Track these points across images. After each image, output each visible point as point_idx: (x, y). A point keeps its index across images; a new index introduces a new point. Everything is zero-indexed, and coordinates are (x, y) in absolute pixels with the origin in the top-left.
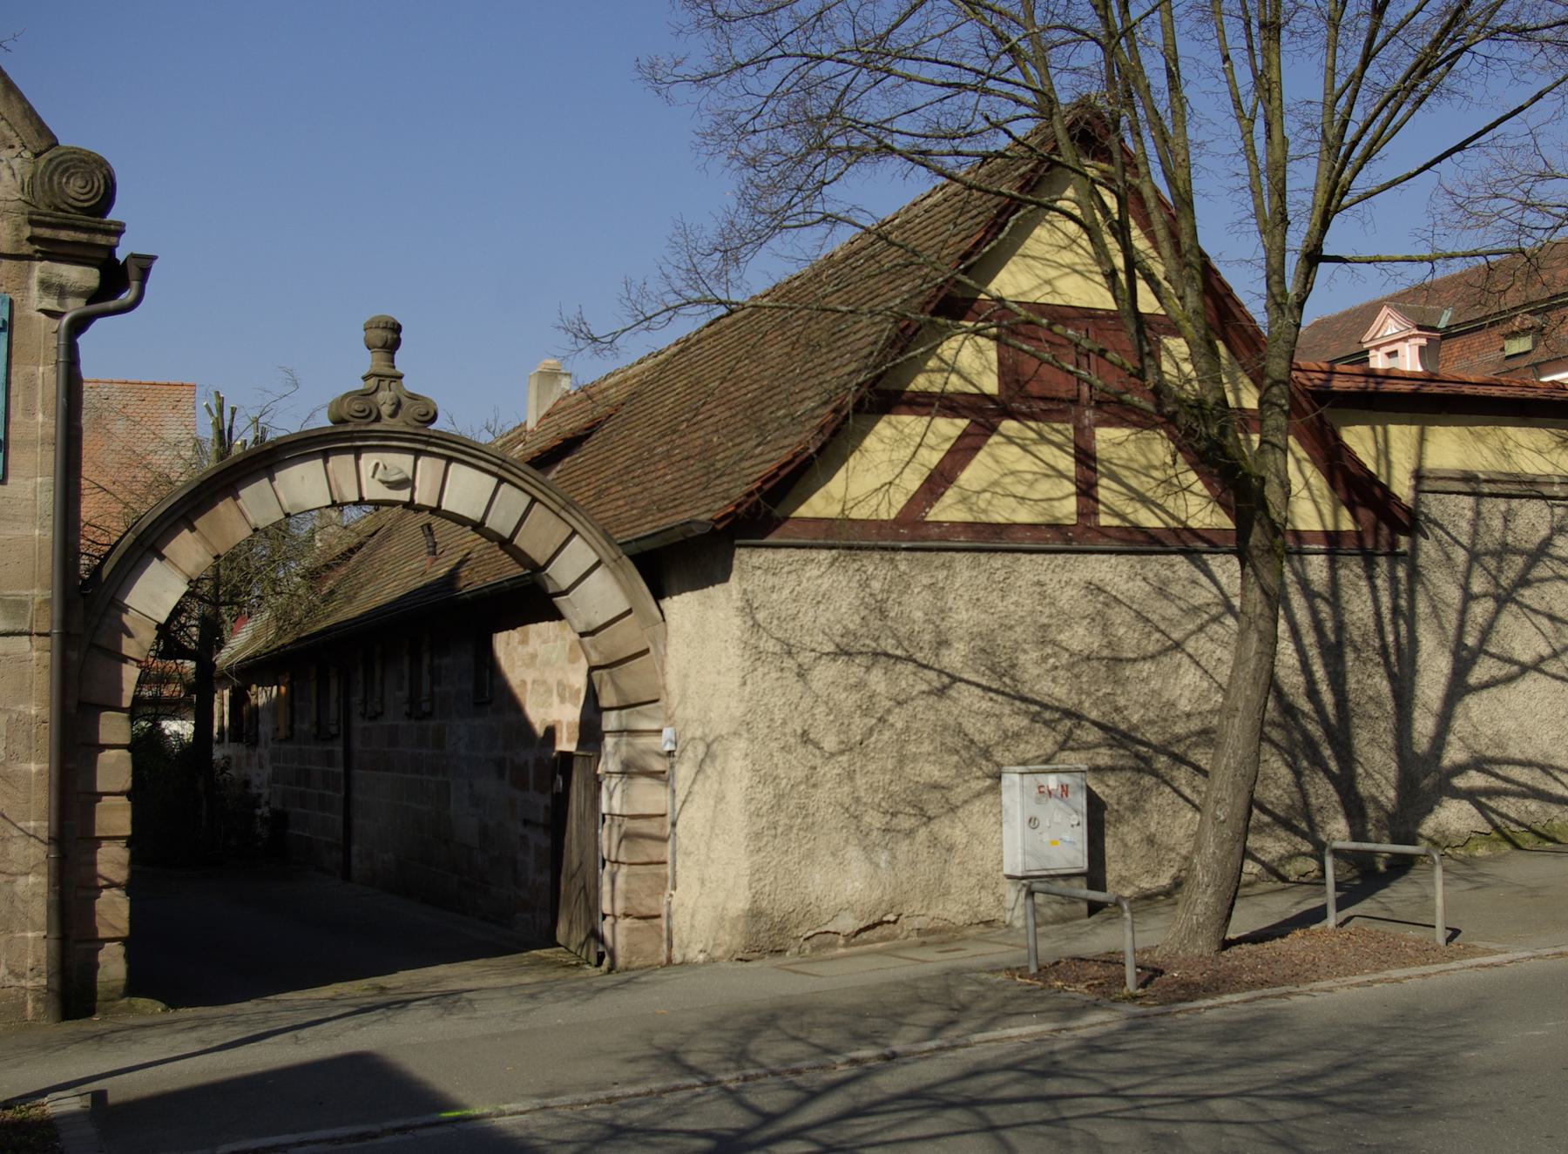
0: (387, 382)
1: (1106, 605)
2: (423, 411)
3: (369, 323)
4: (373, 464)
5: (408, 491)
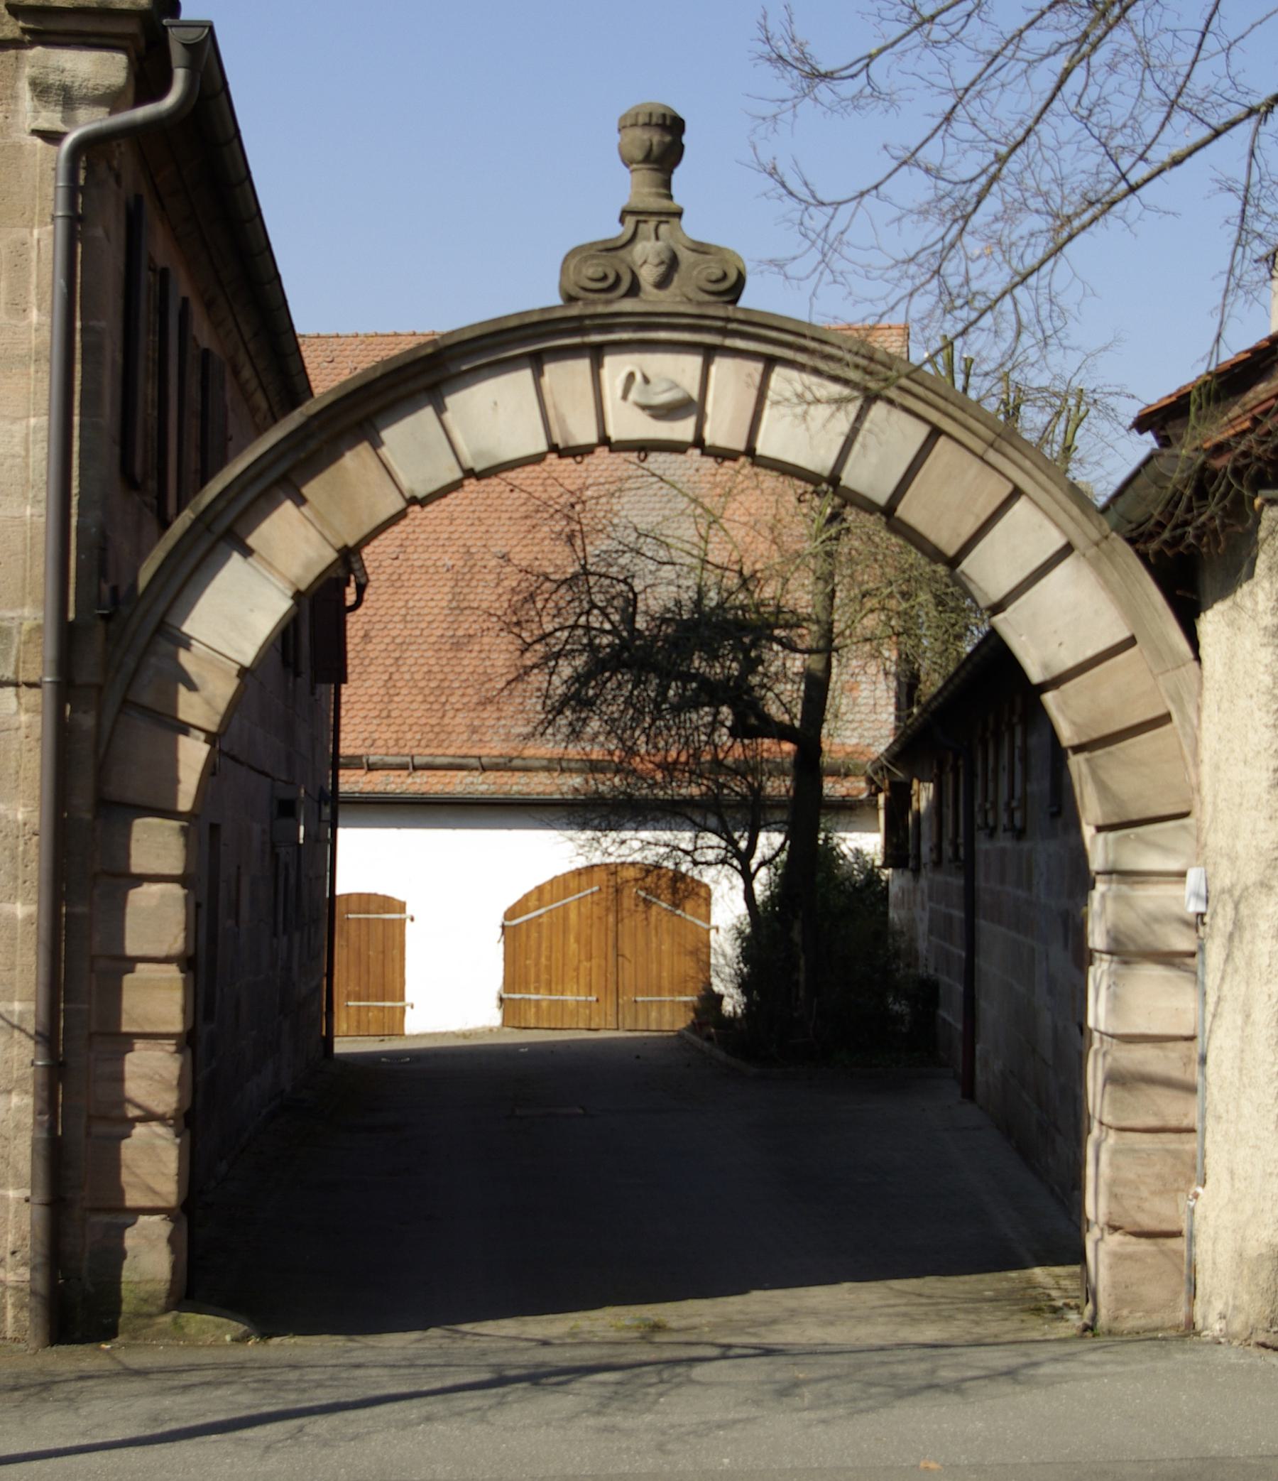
2: (717, 273)
3: (624, 118)
4: (623, 375)
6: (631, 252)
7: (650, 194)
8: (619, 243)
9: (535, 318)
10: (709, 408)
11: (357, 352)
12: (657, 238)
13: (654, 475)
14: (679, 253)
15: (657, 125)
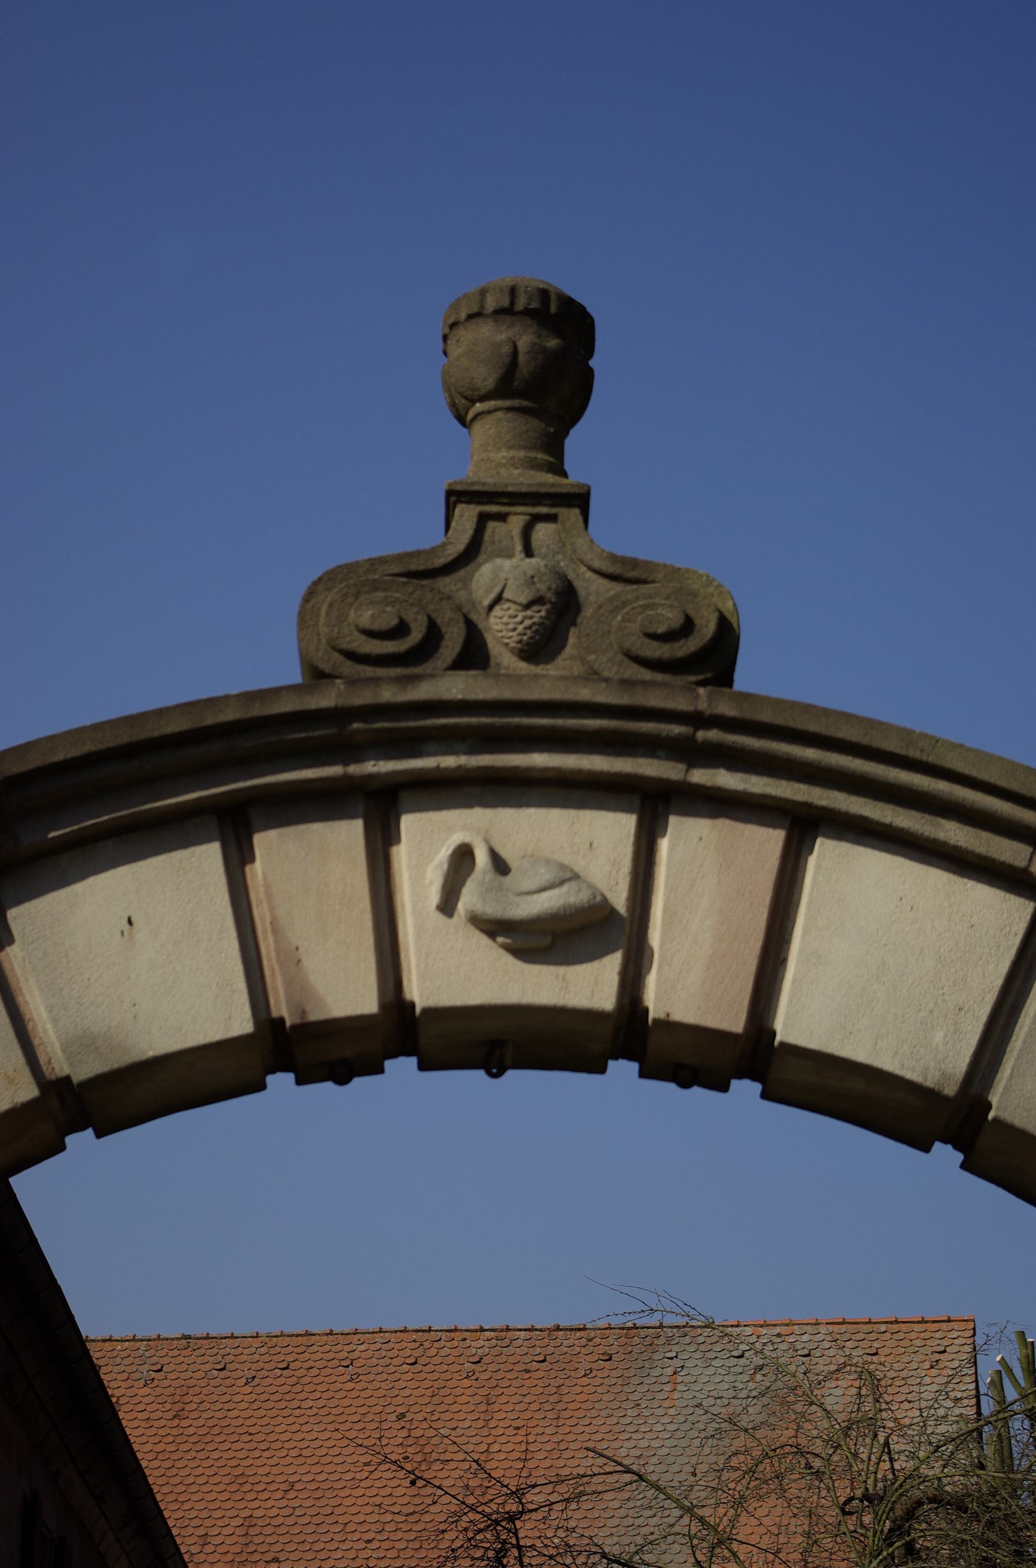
0: (516, 523)
1: (787, 1529)
2: (669, 618)
3: (456, 306)
4: (444, 852)
5: (610, 967)
6: (466, 583)
7: (513, 463)
8: (440, 561)
9: (231, 714)
10: (655, 937)
11: (256, 1357)
12: (529, 552)
13: (628, 1471)
14: (578, 584)
15: (527, 312)
